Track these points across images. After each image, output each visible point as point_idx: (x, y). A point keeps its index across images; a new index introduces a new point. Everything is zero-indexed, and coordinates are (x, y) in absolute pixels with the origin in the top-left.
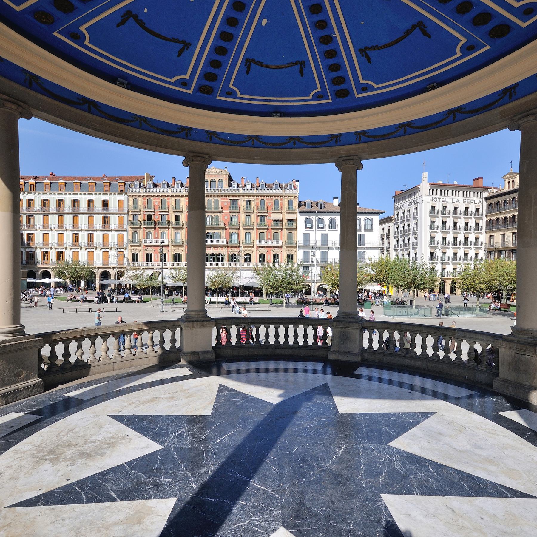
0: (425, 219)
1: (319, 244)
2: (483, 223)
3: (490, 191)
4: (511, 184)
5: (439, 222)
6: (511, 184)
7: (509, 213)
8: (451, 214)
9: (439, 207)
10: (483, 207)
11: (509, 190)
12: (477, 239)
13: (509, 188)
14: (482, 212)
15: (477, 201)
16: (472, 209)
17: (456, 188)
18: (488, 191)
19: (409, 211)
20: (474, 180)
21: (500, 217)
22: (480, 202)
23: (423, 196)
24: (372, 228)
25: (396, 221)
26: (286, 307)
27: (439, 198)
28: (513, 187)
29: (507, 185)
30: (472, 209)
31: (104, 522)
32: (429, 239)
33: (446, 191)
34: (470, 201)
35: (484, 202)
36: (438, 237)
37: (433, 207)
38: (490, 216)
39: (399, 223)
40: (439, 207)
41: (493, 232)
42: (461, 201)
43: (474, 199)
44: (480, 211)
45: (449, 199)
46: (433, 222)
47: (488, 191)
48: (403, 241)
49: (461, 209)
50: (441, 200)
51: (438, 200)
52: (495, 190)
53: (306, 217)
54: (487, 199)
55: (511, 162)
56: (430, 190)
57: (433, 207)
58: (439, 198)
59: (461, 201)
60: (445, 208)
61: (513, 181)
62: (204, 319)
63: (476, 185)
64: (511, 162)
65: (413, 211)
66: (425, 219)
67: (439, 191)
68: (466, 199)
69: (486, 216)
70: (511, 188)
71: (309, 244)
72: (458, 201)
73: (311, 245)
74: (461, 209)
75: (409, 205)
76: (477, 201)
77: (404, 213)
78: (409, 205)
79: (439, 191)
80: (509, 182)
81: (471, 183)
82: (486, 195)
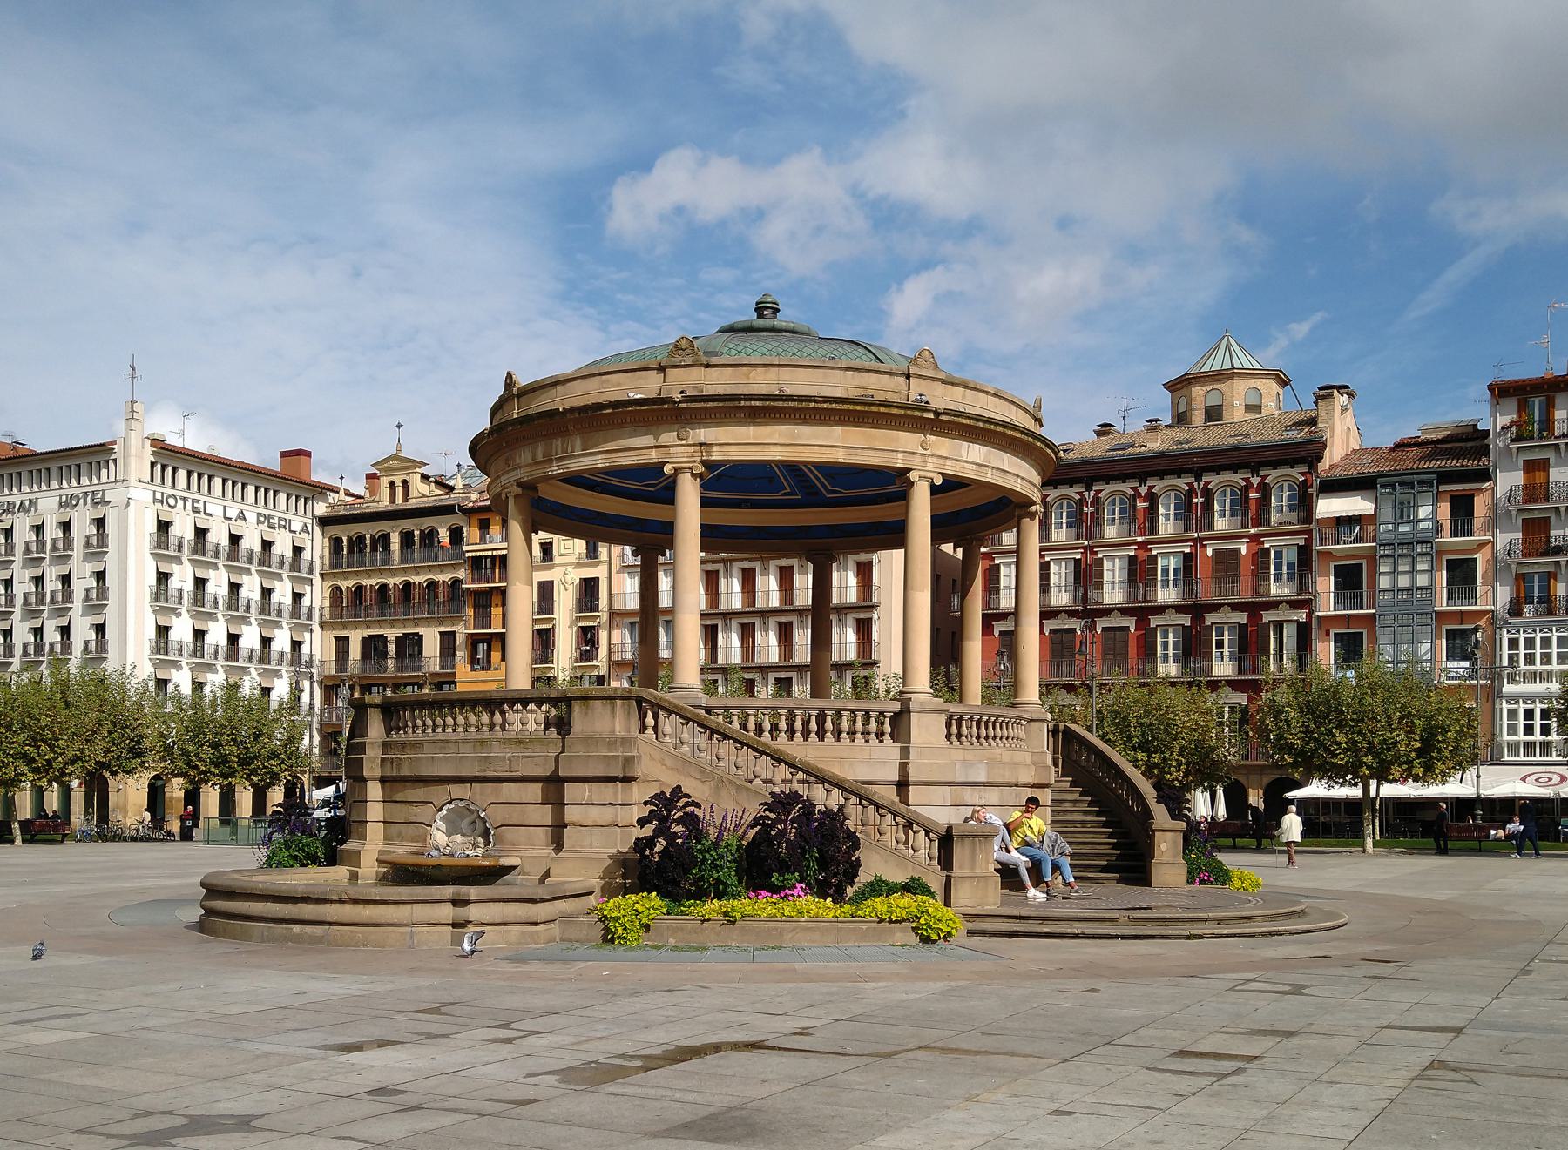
0: (135, 568)
2: (317, 596)
4: (399, 491)
5: (183, 578)
6: (399, 491)
7: (393, 576)
8: (186, 548)
9: (183, 528)
10: (317, 547)
11: (394, 507)
14: (312, 562)
16: (283, 547)
17: (237, 473)
18: (326, 499)
19: (66, 527)
20: (284, 455)
22: (305, 530)
23: (132, 481)
26: (24, 841)
27: (185, 499)
29: (386, 493)
30: (283, 547)
32: (152, 634)
34: (276, 521)
35: (317, 529)
36: (181, 630)
37: (163, 526)
38: (334, 575)
40: (183, 528)
42: (251, 517)
43: (287, 517)
44: (306, 555)
45: (215, 508)
47: (326, 499)
48: (38, 632)
49: (251, 542)
50: (189, 504)
51: (180, 503)
52: (348, 499)
54: (324, 522)
55: (399, 426)
56: (153, 464)
57: (163, 526)
58: (185, 499)
59: (251, 517)
60: (201, 533)
61: (405, 482)
62: (481, 795)
63: (290, 473)
64: (399, 426)
65: (82, 527)
66: (135, 568)
67: (182, 474)
68: (267, 512)
69: (322, 575)
74: (251, 542)
75: (68, 503)
76: (296, 526)
77: (39, 529)
78: (68, 503)
79: (182, 474)
80: (392, 484)
81: (275, 465)
82: (321, 509)
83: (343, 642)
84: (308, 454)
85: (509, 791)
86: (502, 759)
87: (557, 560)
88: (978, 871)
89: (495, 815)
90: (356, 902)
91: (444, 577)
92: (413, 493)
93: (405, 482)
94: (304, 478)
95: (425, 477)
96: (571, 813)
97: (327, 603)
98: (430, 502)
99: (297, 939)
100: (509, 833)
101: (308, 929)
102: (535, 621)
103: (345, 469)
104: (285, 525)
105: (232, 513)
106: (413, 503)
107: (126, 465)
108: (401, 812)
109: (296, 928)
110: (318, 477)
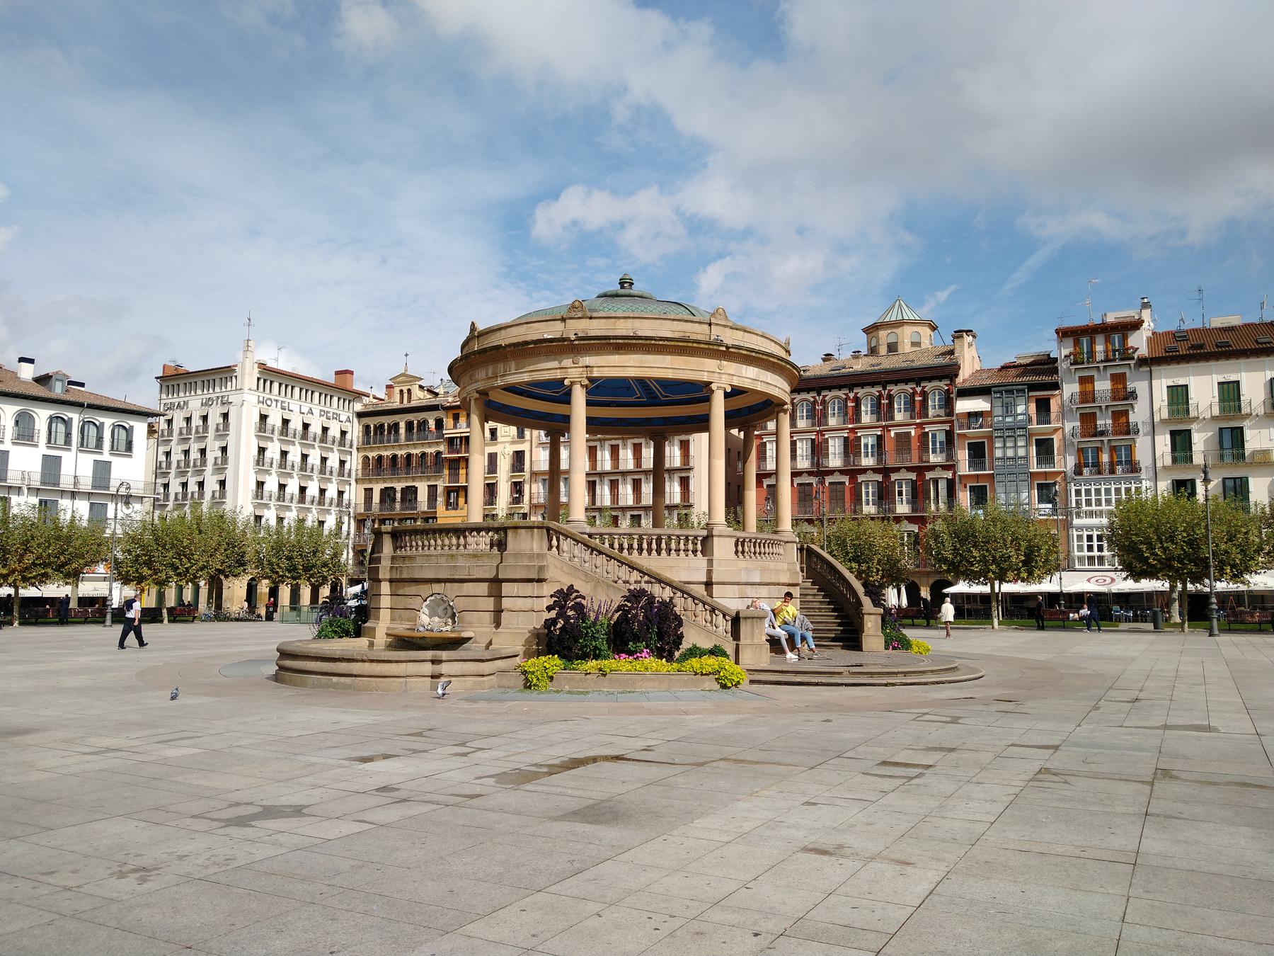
1: (86, 485)
2: (354, 463)
3: (366, 400)
4: (406, 395)
5: (273, 452)
6: (406, 395)
8: (276, 432)
9: (275, 420)
10: (355, 432)
12: (341, 493)
13: (402, 402)
15: (343, 418)
16: (334, 432)
19: (205, 418)
20: (337, 373)
21: (414, 451)
22: (348, 420)
24: (129, 447)
25: (163, 435)
26: (169, 621)
28: (409, 401)
30: (334, 432)
31: (809, 635)
32: (254, 486)
33: (268, 383)
35: (356, 420)
36: (271, 485)
37: (263, 418)
39: (173, 444)
40: (275, 420)
41: (414, 479)
42: (316, 412)
45: (294, 406)
46: (262, 450)
53: (52, 412)
54: (360, 415)
56: (259, 379)
57: (263, 418)
59: (316, 412)
60: (286, 422)
61: (409, 391)
62: (451, 590)
63: (340, 385)
65: (215, 419)
66: (244, 442)
67: (276, 385)
70: (406, 404)
71: (108, 488)
72: (311, 412)
73: (113, 490)
76: (343, 418)
77: (188, 420)
79: (276, 385)
80: (401, 391)
81: (331, 379)
82: (358, 407)
83: (369, 492)
84: (352, 373)
85: (468, 588)
86: (464, 567)
87: (500, 439)
88: (756, 641)
89: (459, 604)
90: (372, 661)
91: (431, 450)
92: (414, 397)
93: (409, 391)
94: (349, 388)
95: (421, 387)
96: (506, 603)
97: (360, 467)
98: (424, 403)
99: (335, 686)
100: (467, 616)
101: (342, 679)
102: (486, 478)
103: (373, 383)
104: (336, 417)
105: (305, 410)
106: (414, 403)
107: (243, 379)
108: (401, 602)
109: (335, 679)
110: (357, 387)
